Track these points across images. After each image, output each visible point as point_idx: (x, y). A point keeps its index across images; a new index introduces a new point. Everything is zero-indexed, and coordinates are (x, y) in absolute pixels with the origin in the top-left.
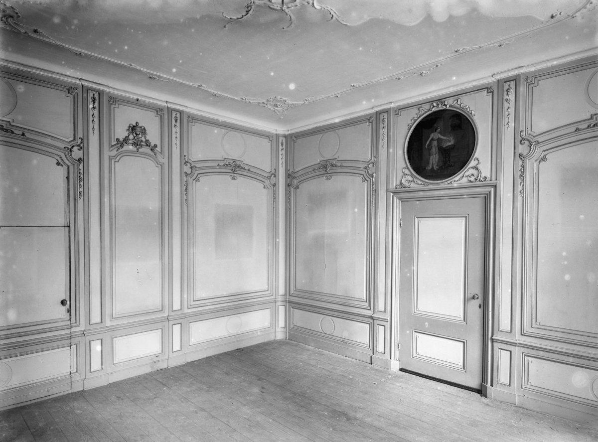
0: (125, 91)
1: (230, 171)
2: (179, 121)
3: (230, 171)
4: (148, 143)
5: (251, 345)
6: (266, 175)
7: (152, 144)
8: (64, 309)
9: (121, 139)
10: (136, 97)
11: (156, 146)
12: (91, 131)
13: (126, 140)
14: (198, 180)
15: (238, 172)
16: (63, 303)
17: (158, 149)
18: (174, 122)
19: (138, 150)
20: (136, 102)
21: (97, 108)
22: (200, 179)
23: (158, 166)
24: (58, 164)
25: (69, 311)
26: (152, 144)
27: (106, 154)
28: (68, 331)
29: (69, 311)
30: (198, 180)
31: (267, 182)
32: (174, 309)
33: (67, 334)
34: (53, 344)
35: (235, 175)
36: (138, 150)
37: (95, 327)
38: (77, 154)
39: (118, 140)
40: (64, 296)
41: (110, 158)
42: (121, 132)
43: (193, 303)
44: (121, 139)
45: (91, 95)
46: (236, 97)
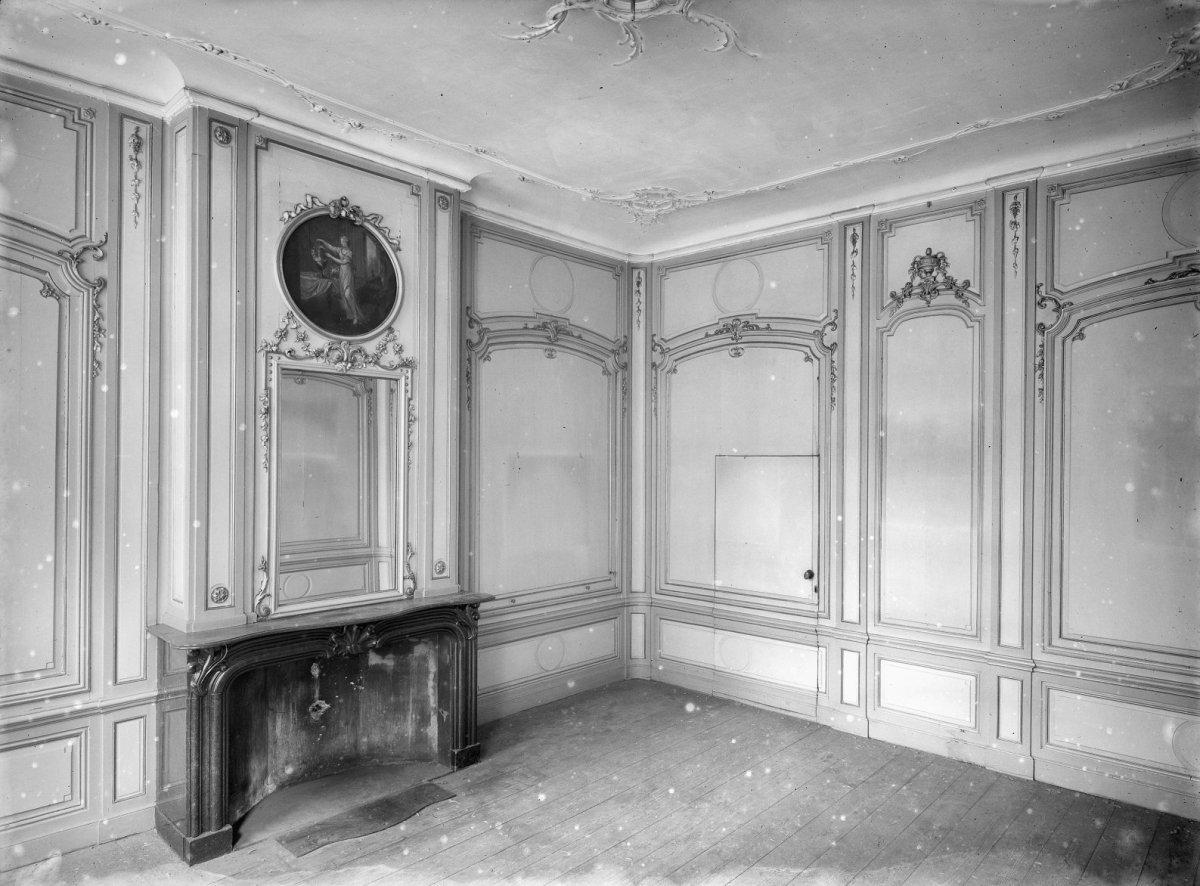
0: (678, 250)
1: (730, 341)
2: (1022, 209)
3: (730, 341)
4: (950, 284)
5: (694, 689)
6: (610, 347)
7: (959, 283)
8: (809, 585)
9: (899, 292)
10: (923, 201)
11: (967, 283)
12: (635, 325)
13: (908, 292)
14: (1081, 336)
15: (744, 339)
16: (810, 575)
17: (974, 288)
18: (1009, 217)
19: (928, 302)
20: (928, 209)
21: (860, 251)
22: (1085, 332)
23: (972, 324)
24: (808, 359)
25: (817, 590)
26: (959, 283)
27: (875, 324)
28: (813, 622)
29: (817, 590)
30: (1081, 336)
31: (610, 362)
32: (857, 621)
33: (812, 626)
34: (747, 627)
35: (739, 346)
36: (928, 302)
37: (849, 627)
38: (831, 336)
39: (893, 295)
40: (809, 564)
41: (881, 332)
42: (898, 275)
43: (664, 587)
44: (899, 292)
45: (850, 232)
46: (1100, 93)
